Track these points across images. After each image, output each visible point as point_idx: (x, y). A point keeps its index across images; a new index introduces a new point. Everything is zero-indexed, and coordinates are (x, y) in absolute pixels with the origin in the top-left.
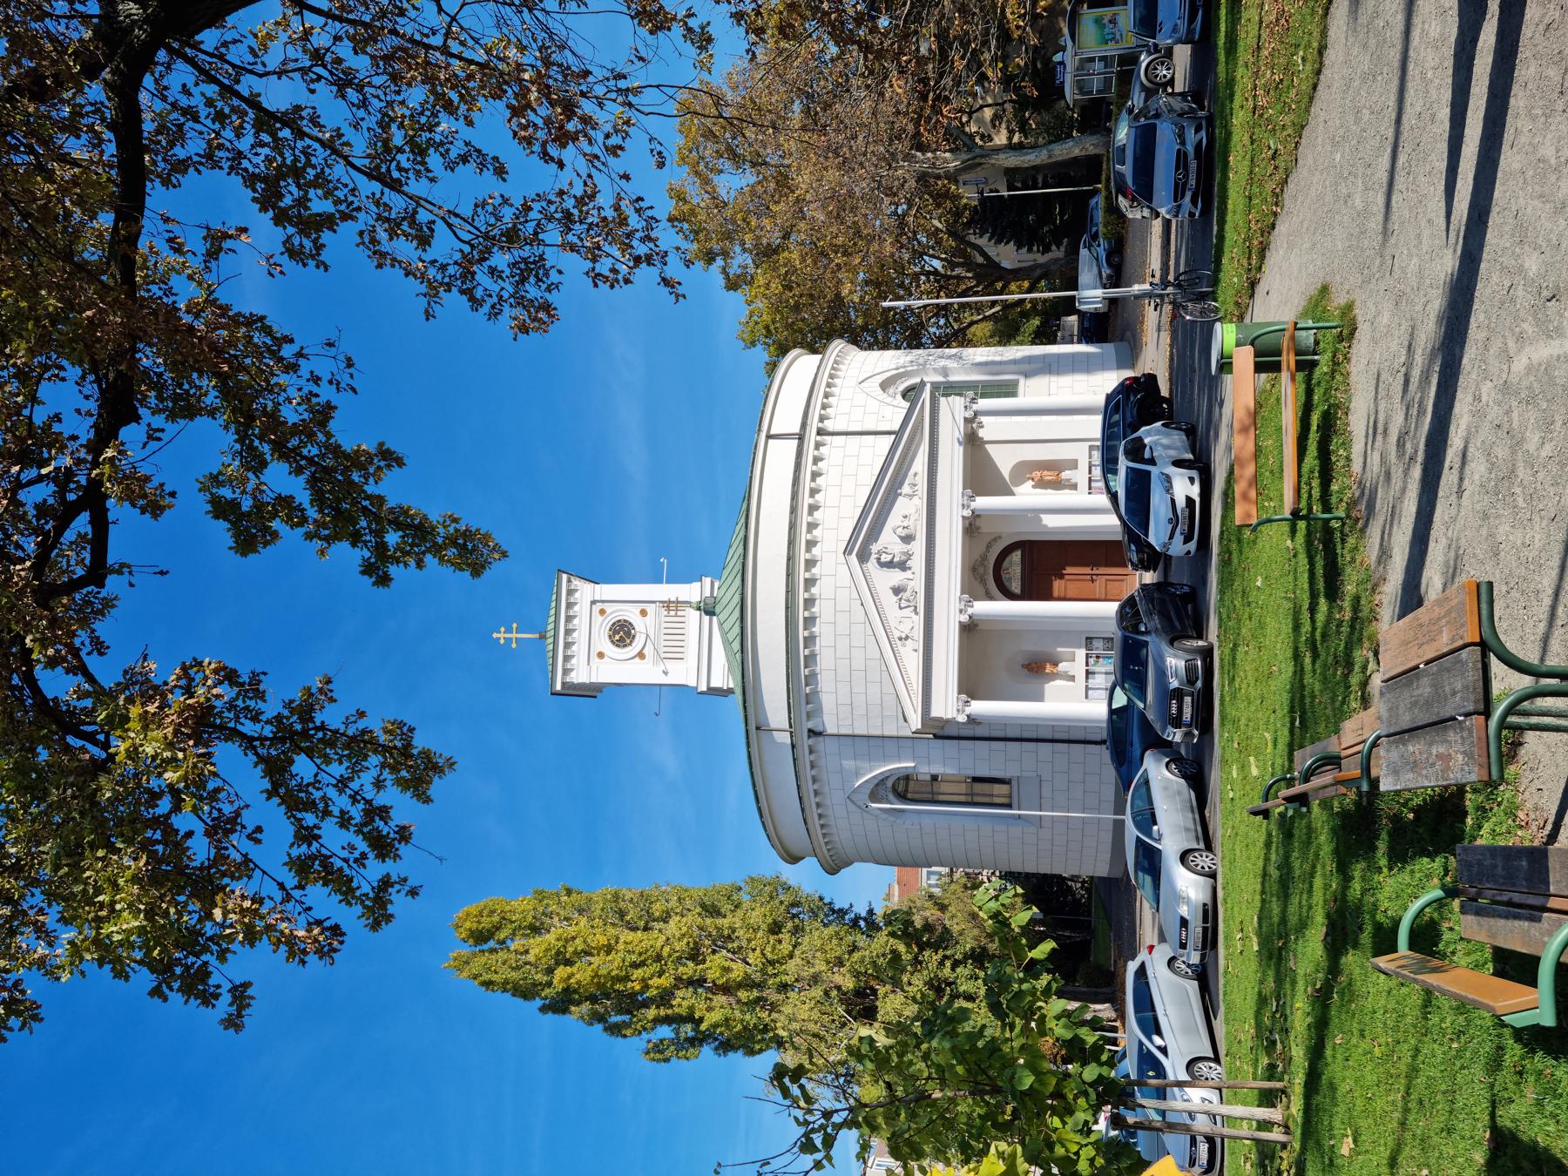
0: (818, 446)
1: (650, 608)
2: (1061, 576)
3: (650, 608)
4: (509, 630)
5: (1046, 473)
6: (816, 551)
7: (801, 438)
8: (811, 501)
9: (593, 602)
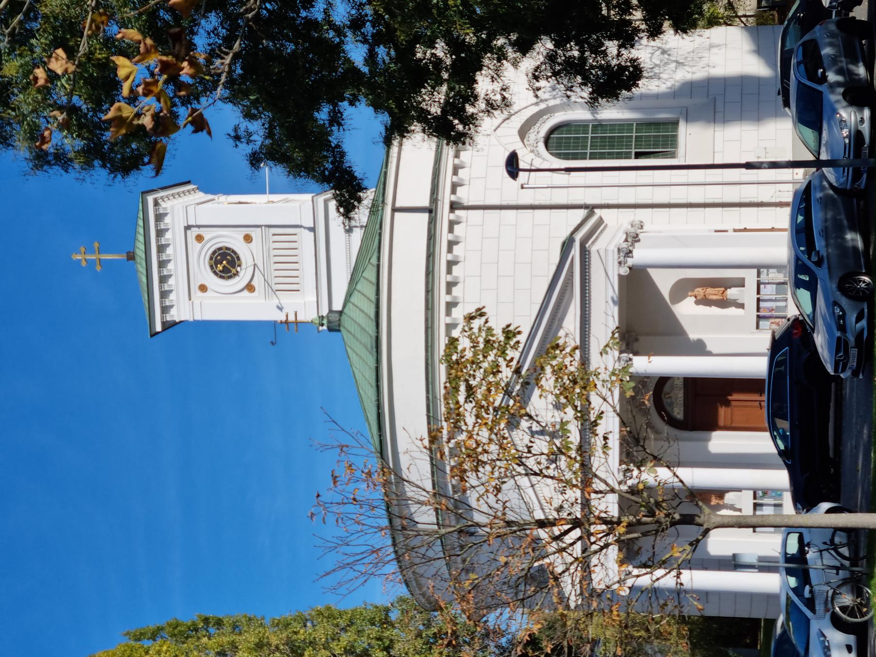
0: (452, 224)
1: (255, 233)
2: (727, 403)
3: (255, 233)
4: (89, 250)
5: (710, 290)
6: (456, 291)
7: (431, 211)
8: (448, 298)
9: (188, 228)
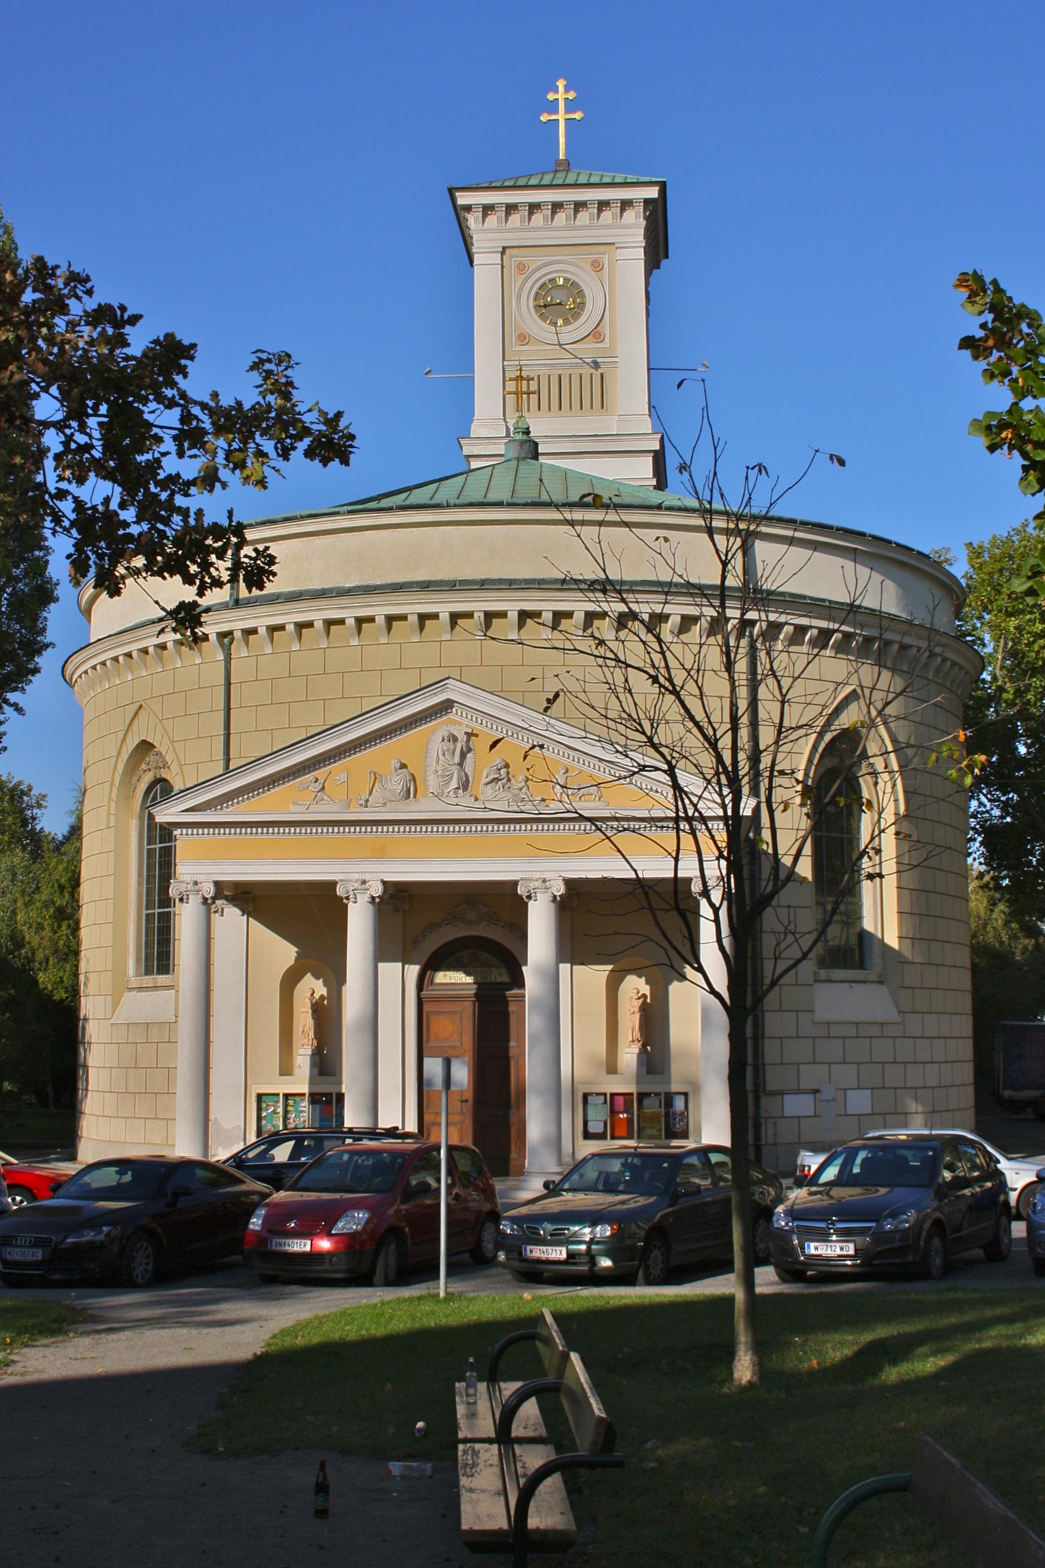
4: (570, 106)
